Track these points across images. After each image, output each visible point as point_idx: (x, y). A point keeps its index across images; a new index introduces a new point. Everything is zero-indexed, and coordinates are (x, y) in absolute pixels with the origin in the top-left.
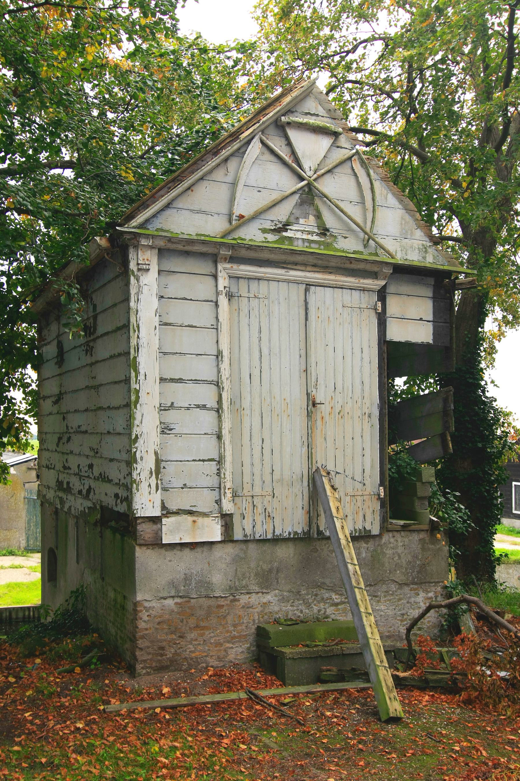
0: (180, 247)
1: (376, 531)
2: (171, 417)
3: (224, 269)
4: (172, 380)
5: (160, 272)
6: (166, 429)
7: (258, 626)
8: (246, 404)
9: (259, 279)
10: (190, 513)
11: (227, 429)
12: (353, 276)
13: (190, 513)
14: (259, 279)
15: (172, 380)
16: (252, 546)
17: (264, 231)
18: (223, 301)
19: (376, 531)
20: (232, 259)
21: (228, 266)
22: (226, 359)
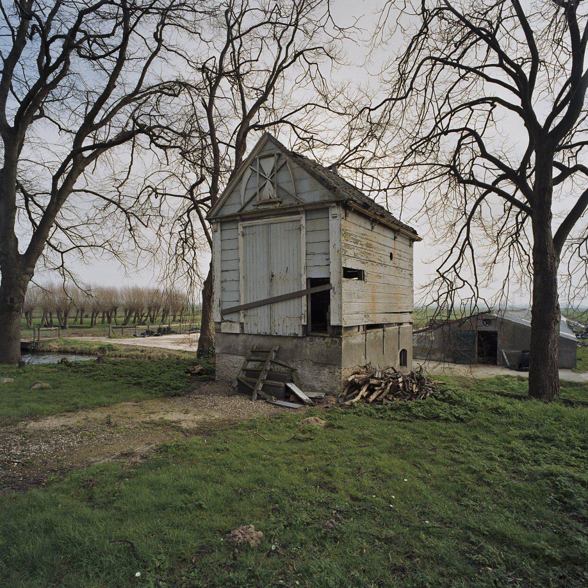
0: (248, 216)
1: (300, 335)
2: (225, 284)
3: (240, 225)
4: (226, 271)
5: (306, 220)
6: (223, 290)
7: (258, 378)
8: (248, 278)
9: (252, 226)
10: (230, 322)
11: (521, 431)
12: (295, 215)
13: (230, 322)
14: (252, 226)
15: (226, 271)
16: (251, 336)
17: (254, 205)
18: (241, 238)
19: (300, 335)
20: (243, 220)
21: (241, 223)
22: (241, 261)
